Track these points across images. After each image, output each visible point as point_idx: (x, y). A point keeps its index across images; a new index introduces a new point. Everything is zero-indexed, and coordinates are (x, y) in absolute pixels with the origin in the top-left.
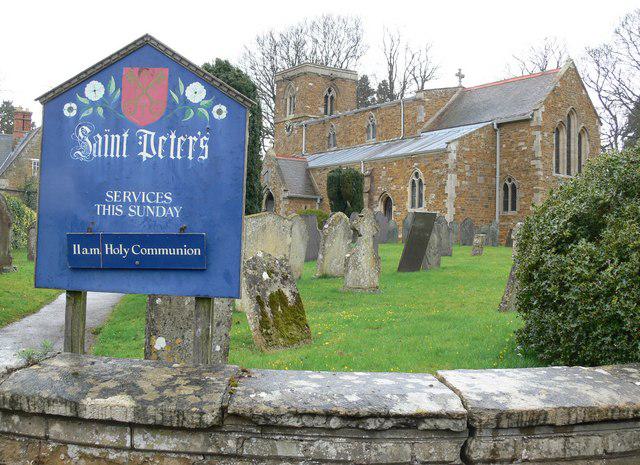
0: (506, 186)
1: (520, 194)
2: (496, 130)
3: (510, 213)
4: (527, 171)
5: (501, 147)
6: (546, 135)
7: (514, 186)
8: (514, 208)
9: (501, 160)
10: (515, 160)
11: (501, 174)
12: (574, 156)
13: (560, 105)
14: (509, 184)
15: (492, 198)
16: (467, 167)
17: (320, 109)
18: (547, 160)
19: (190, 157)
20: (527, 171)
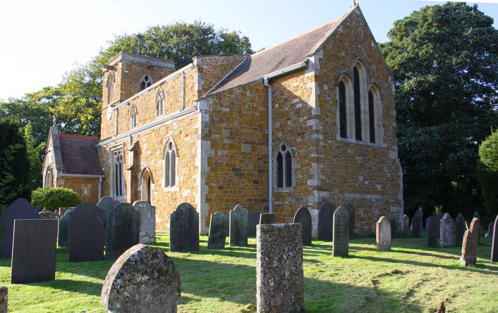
0: (280, 157)
1: (295, 166)
2: (267, 87)
3: (285, 190)
4: (302, 135)
5: (273, 107)
6: (326, 87)
7: (288, 155)
8: (289, 184)
9: (273, 123)
10: (289, 122)
11: (273, 141)
12: (365, 118)
13: (343, 54)
14: (283, 153)
15: (263, 171)
16: (225, 133)
17: (377, 186)
18: (328, 120)
19: (133, 205)
20: (302, 135)
